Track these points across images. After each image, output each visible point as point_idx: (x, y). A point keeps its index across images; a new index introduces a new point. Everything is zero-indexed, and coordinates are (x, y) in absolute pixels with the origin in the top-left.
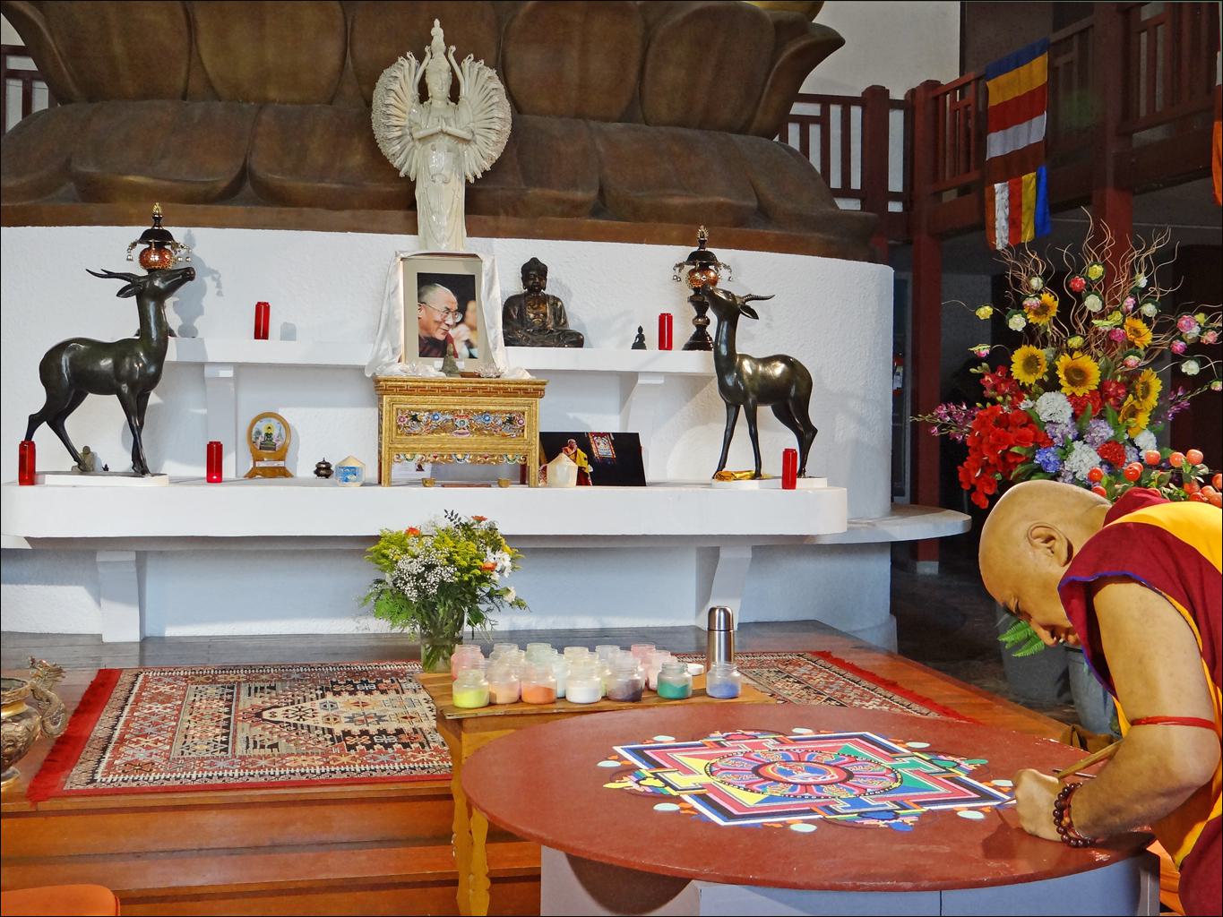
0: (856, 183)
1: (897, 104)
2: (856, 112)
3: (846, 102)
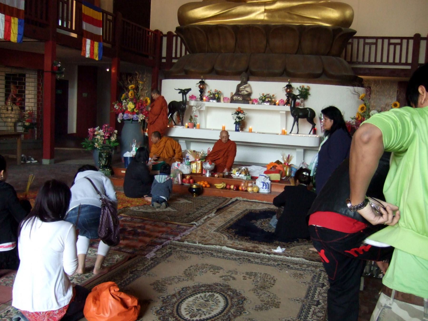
0: (410, 61)
1: (165, 36)
2: (411, 42)
3: (408, 39)
